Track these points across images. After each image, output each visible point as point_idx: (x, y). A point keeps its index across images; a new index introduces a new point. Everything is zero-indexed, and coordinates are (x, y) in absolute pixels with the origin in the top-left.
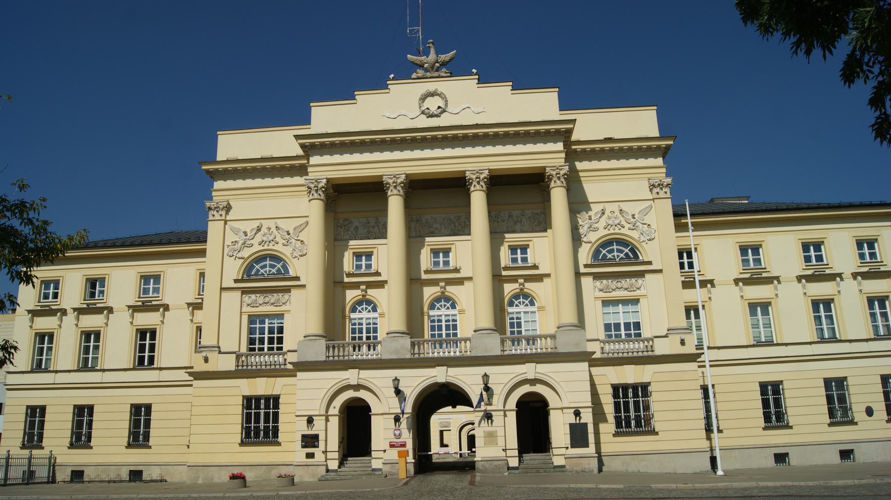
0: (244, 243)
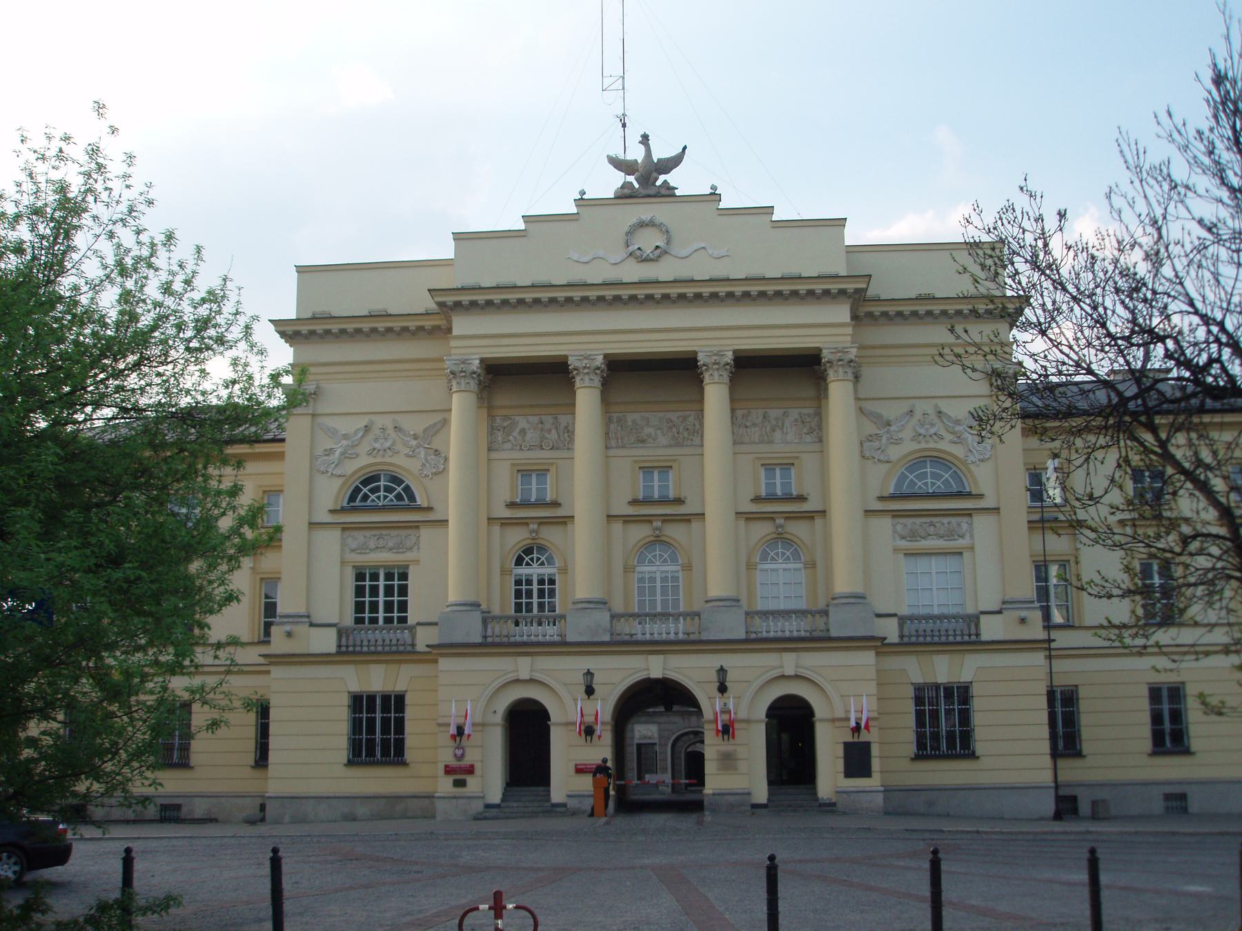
0: (342, 454)
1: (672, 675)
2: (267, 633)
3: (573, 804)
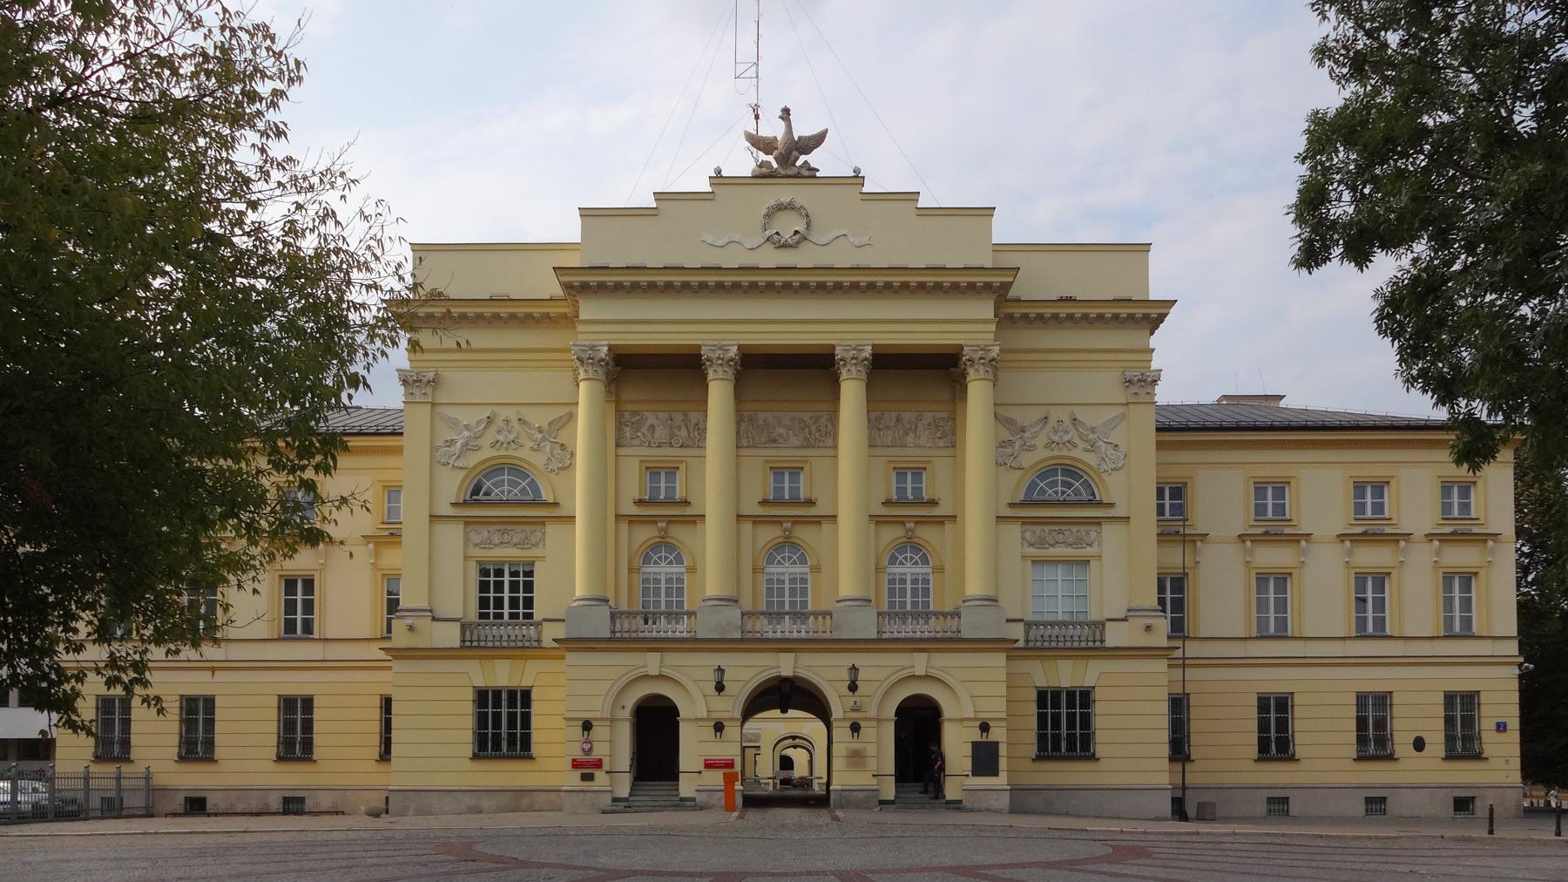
0: (466, 444)
1: (803, 673)
2: (389, 630)
3: (701, 798)
